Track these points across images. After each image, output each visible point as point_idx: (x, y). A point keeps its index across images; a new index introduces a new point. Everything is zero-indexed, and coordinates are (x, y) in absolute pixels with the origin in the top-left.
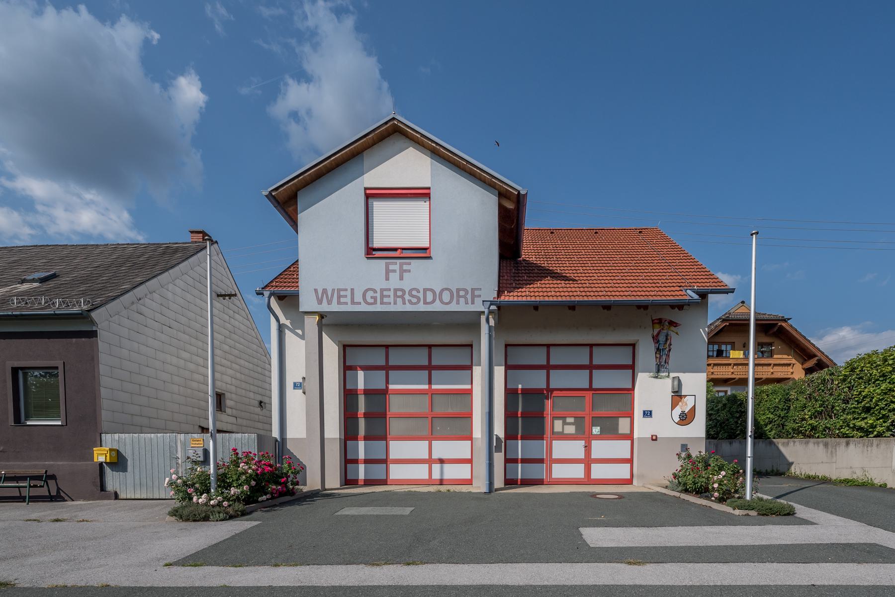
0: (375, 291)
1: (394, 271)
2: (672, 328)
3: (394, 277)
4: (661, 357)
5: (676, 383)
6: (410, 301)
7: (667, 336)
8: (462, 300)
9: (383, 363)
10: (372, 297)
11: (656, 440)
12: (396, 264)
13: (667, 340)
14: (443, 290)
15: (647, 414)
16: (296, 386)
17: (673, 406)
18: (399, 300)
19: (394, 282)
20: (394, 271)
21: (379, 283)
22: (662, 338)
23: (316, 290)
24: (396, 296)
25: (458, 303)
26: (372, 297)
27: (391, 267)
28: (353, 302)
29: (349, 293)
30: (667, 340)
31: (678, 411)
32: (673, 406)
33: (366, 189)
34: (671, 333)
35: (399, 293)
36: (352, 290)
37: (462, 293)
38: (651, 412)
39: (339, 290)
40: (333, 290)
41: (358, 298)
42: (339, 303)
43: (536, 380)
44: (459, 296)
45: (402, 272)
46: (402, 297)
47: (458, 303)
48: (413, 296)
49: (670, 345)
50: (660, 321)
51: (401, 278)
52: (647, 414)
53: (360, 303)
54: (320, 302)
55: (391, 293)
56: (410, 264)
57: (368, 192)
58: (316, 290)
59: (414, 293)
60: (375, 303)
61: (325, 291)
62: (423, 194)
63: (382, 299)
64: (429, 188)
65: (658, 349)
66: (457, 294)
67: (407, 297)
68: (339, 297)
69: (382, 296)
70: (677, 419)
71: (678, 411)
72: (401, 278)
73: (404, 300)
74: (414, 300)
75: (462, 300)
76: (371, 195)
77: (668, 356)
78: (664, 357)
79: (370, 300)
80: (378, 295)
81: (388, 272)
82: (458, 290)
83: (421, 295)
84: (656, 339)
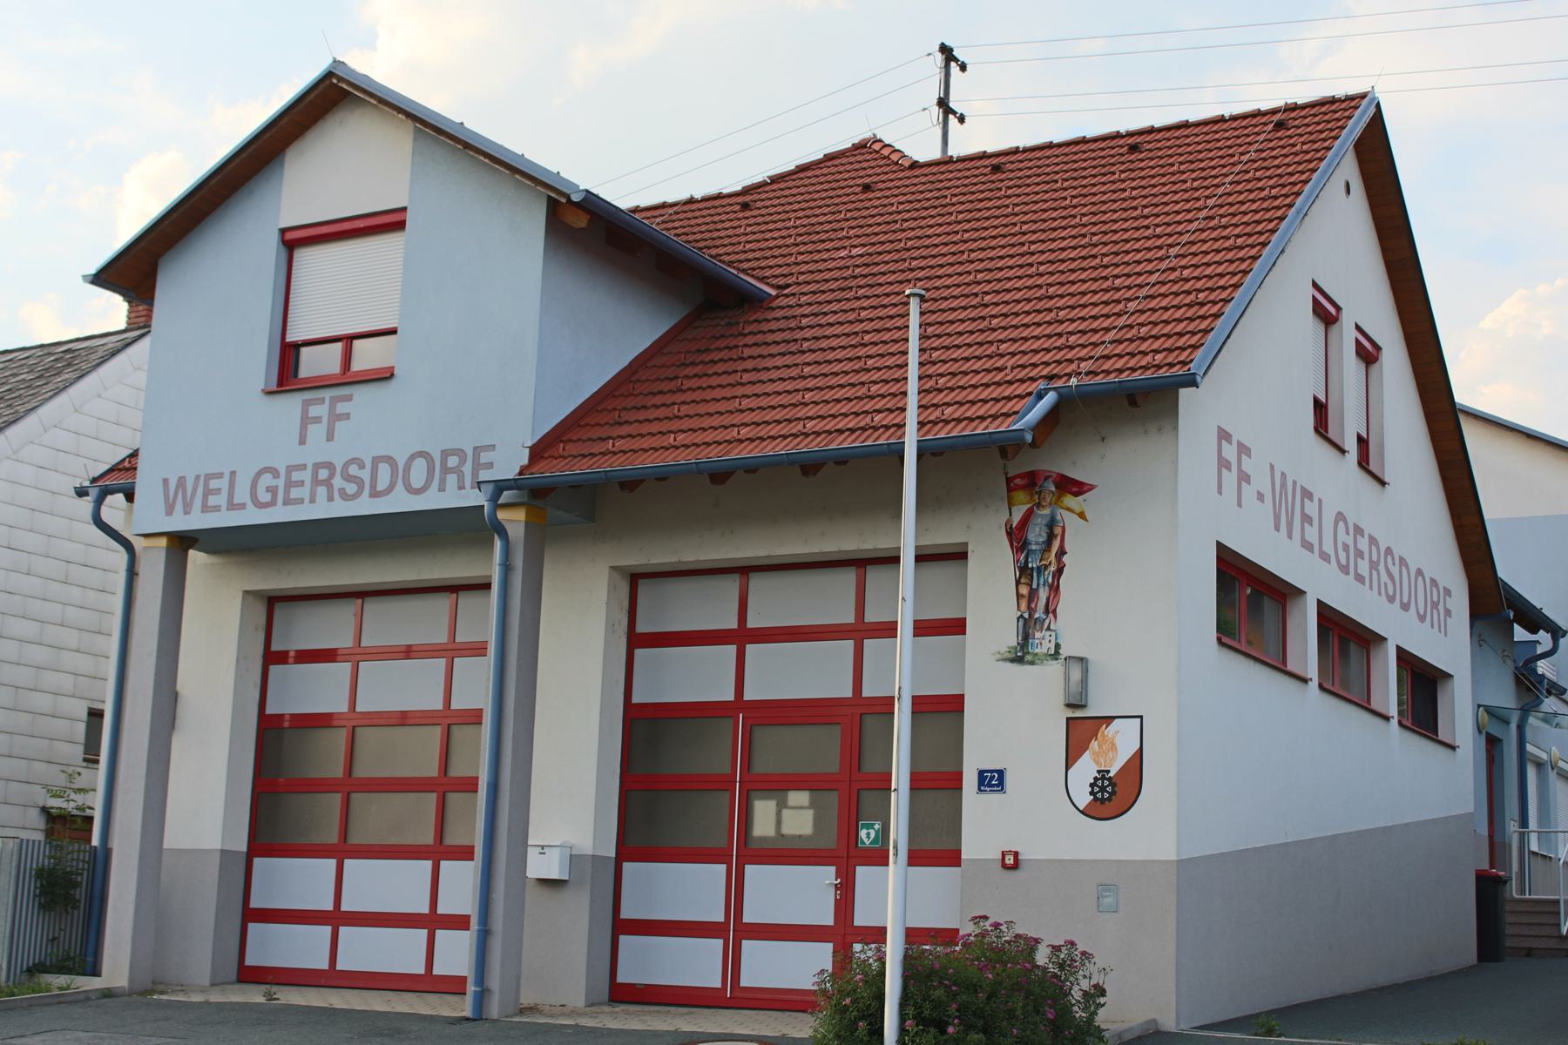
0: (275, 473)
1: (318, 420)
2: (1069, 500)
3: (316, 432)
4: (1033, 594)
5: (1076, 674)
6: (342, 492)
7: (1051, 524)
8: (452, 479)
9: (441, 637)
10: (268, 489)
11: (1016, 866)
12: (322, 401)
13: (1051, 537)
14: (413, 457)
15: (992, 780)
16: (470, 785)
17: (1072, 754)
18: (322, 491)
19: (317, 448)
20: (318, 420)
21: (285, 453)
22: (1036, 535)
23: (166, 481)
24: (316, 482)
25: (442, 489)
26: (268, 489)
27: (314, 411)
28: (232, 506)
29: (223, 484)
30: (1051, 537)
31: (1086, 769)
32: (1072, 754)
33: (283, 231)
34: (1062, 514)
35: (323, 474)
36: (233, 473)
37: (453, 461)
38: (1001, 773)
39: (209, 477)
40: (197, 478)
41: (242, 495)
42: (205, 508)
43: (700, 677)
44: (446, 470)
45: (335, 418)
46: (328, 483)
47: (442, 489)
48: (349, 478)
49: (1062, 552)
50: (1032, 481)
51: (330, 437)
52: (992, 780)
53: (242, 506)
54: (170, 510)
55: (306, 476)
56: (349, 398)
57: (289, 236)
58: (166, 481)
59: (353, 470)
60: (273, 503)
61: (182, 481)
62: (390, 223)
63: (287, 492)
64: (404, 209)
65: (1024, 571)
66: (441, 465)
67: (338, 482)
68: (208, 492)
69: (290, 484)
70: (1084, 799)
71: (1086, 769)
72: (330, 437)
73: (330, 487)
74: (351, 488)
75: (452, 479)
76: (294, 241)
77: (1055, 589)
78: (1043, 594)
79: (264, 497)
80: (281, 483)
81: (306, 421)
82: (445, 454)
83: (365, 475)
84: (1017, 537)
